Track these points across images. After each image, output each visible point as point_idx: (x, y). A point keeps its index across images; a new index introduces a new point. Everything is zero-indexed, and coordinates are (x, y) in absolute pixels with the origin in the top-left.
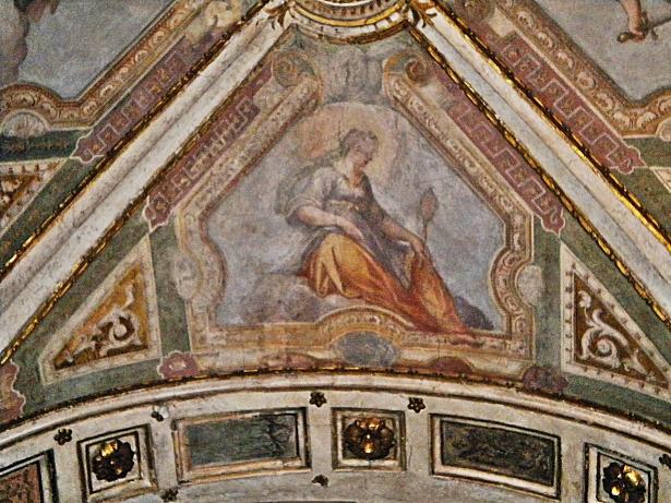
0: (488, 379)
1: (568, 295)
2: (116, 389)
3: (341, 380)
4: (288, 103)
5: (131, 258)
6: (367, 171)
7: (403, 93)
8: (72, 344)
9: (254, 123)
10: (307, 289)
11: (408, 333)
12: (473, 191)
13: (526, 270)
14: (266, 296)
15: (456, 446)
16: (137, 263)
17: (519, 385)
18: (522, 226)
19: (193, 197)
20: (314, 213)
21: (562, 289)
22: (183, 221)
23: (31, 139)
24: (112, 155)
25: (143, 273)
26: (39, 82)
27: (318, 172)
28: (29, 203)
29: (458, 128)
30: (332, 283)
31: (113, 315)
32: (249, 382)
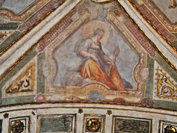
0: (130, 104)
1: (156, 76)
2: (22, 104)
3: (87, 105)
4: (81, 20)
5: (32, 61)
6: (101, 41)
7: (113, 18)
8: (12, 86)
9: (71, 25)
10: (80, 76)
11: (108, 91)
12: (130, 47)
13: (144, 69)
14: (68, 78)
15: (119, 127)
16: (33, 63)
17: (140, 105)
18: (144, 56)
19: (51, 45)
20: (84, 53)
21: (154, 74)
22: (48, 52)
23: (4, 24)
24: (28, 31)
25: (34, 66)
26: (8, 8)
27: (87, 40)
28: (2, 42)
29: (127, 29)
30: (87, 75)
31: (24, 79)
32: (60, 105)
